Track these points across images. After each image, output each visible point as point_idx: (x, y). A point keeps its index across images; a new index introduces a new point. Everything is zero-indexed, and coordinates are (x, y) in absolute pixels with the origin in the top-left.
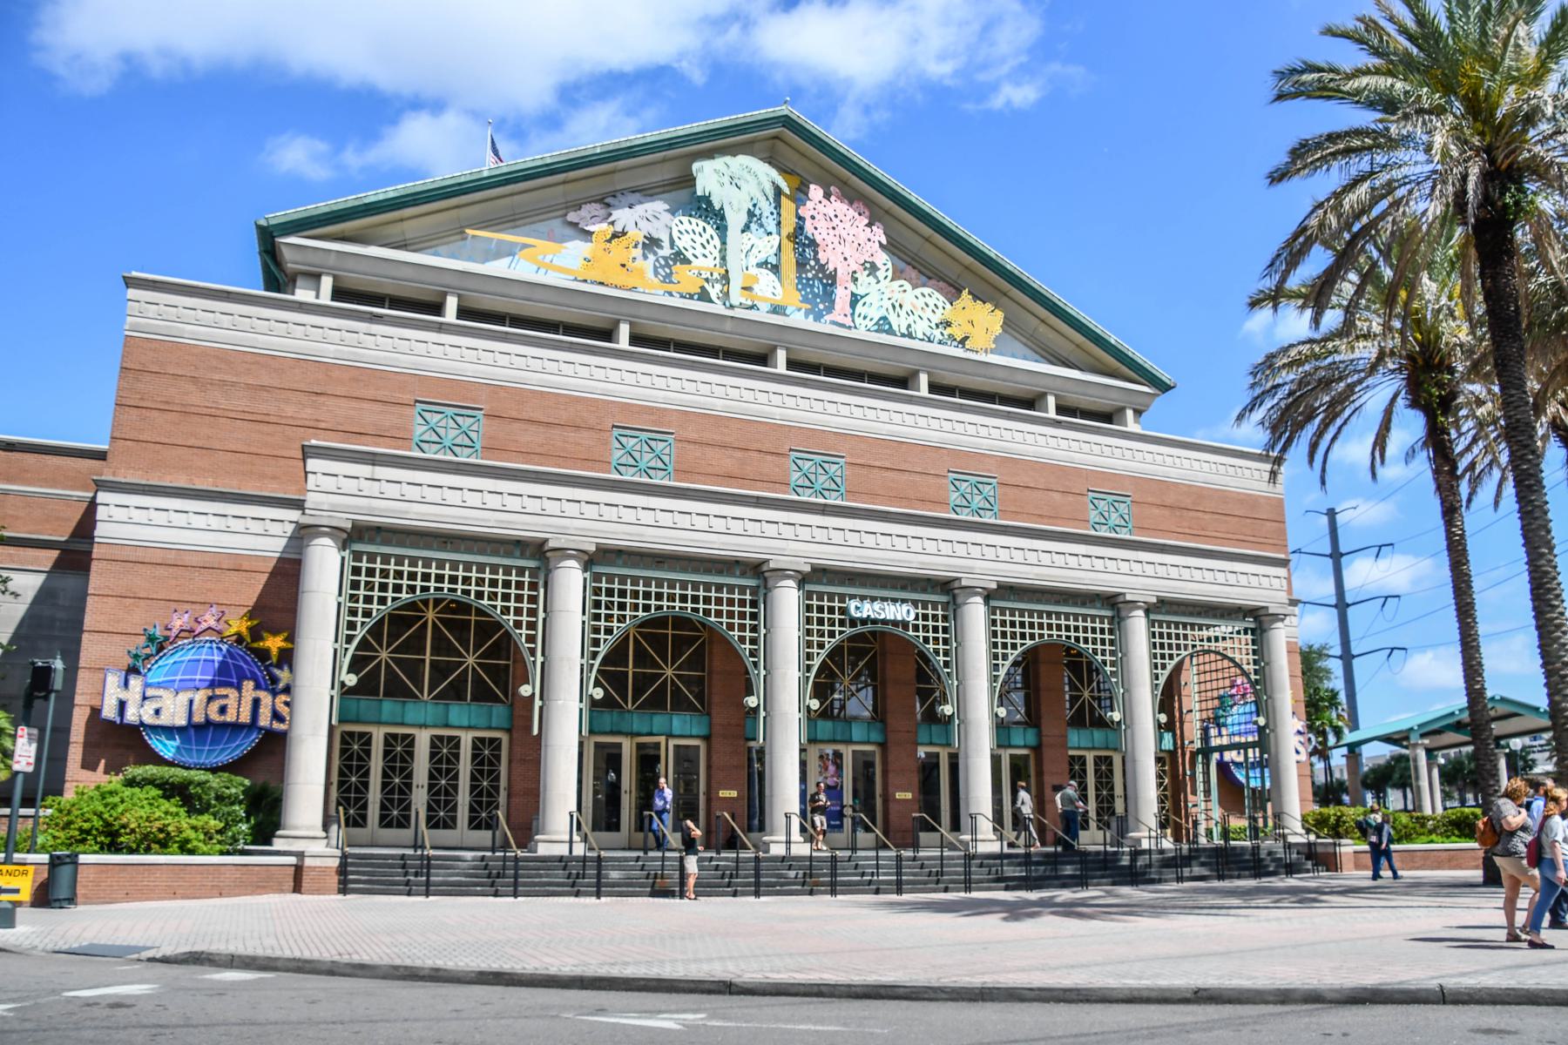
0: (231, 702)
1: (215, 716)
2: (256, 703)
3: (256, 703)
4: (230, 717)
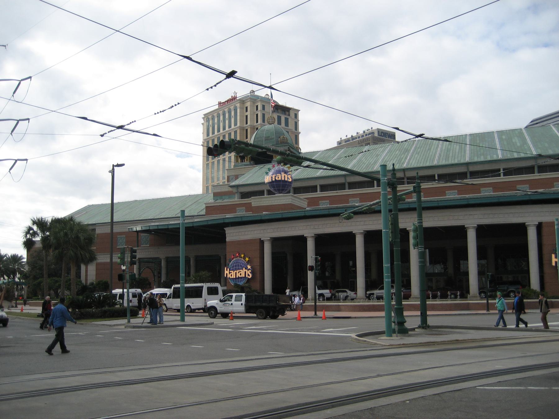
1: (240, 276)
2: (245, 272)
3: (245, 272)
4: (232, 277)
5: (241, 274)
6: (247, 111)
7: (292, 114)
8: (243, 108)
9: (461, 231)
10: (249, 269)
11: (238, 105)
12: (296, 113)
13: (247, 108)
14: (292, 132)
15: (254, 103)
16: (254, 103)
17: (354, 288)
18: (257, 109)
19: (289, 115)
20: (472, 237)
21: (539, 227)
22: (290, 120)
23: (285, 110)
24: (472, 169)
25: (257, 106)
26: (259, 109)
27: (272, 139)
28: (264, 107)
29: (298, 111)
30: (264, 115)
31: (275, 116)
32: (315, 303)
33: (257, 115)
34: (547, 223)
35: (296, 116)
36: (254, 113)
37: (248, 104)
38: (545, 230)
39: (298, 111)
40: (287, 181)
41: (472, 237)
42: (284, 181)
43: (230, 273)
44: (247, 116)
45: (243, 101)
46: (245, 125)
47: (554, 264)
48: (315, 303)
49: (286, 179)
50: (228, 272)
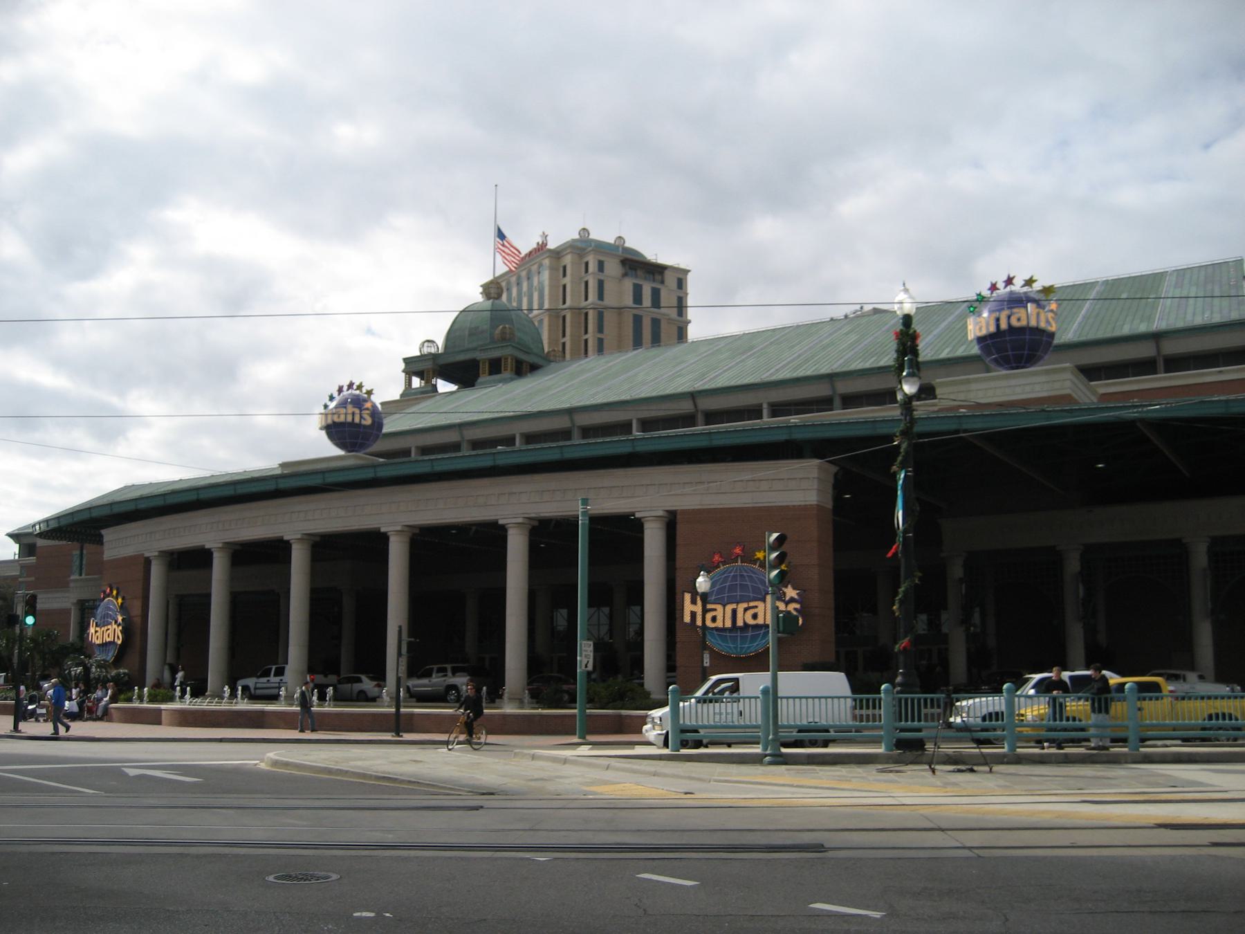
0: (720, 618)
1: (751, 622)
4: (719, 624)
5: (755, 616)
6: (564, 275)
7: (670, 280)
8: (557, 270)
9: (494, 535)
10: (792, 600)
11: (547, 262)
12: (681, 277)
13: (565, 268)
14: (670, 321)
15: (581, 256)
16: (581, 256)
17: (379, 675)
18: (587, 271)
19: (662, 282)
20: (299, 560)
21: (671, 522)
22: (663, 294)
23: (656, 271)
24: (844, 388)
25: (587, 264)
26: (591, 269)
27: (482, 332)
28: (601, 266)
29: (686, 272)
30: (601, 284)
31: (628, 284)
32: (398, 708)
33: (587, 283)
34: (685, 512)
35: (681, 284)
36: (581, 278)
37: (568, 260)
38: (681, 529)
39: (686, 272)
40: (359, 425)
41: (299, 560)
42: (352, 424)
43: (705, 611)
44: (564, 287)
45: (557, 254)
46: (584, 304)
47: (687, 619)
48: (398, 708)
49: (357, 420)
50: (698, 609)
